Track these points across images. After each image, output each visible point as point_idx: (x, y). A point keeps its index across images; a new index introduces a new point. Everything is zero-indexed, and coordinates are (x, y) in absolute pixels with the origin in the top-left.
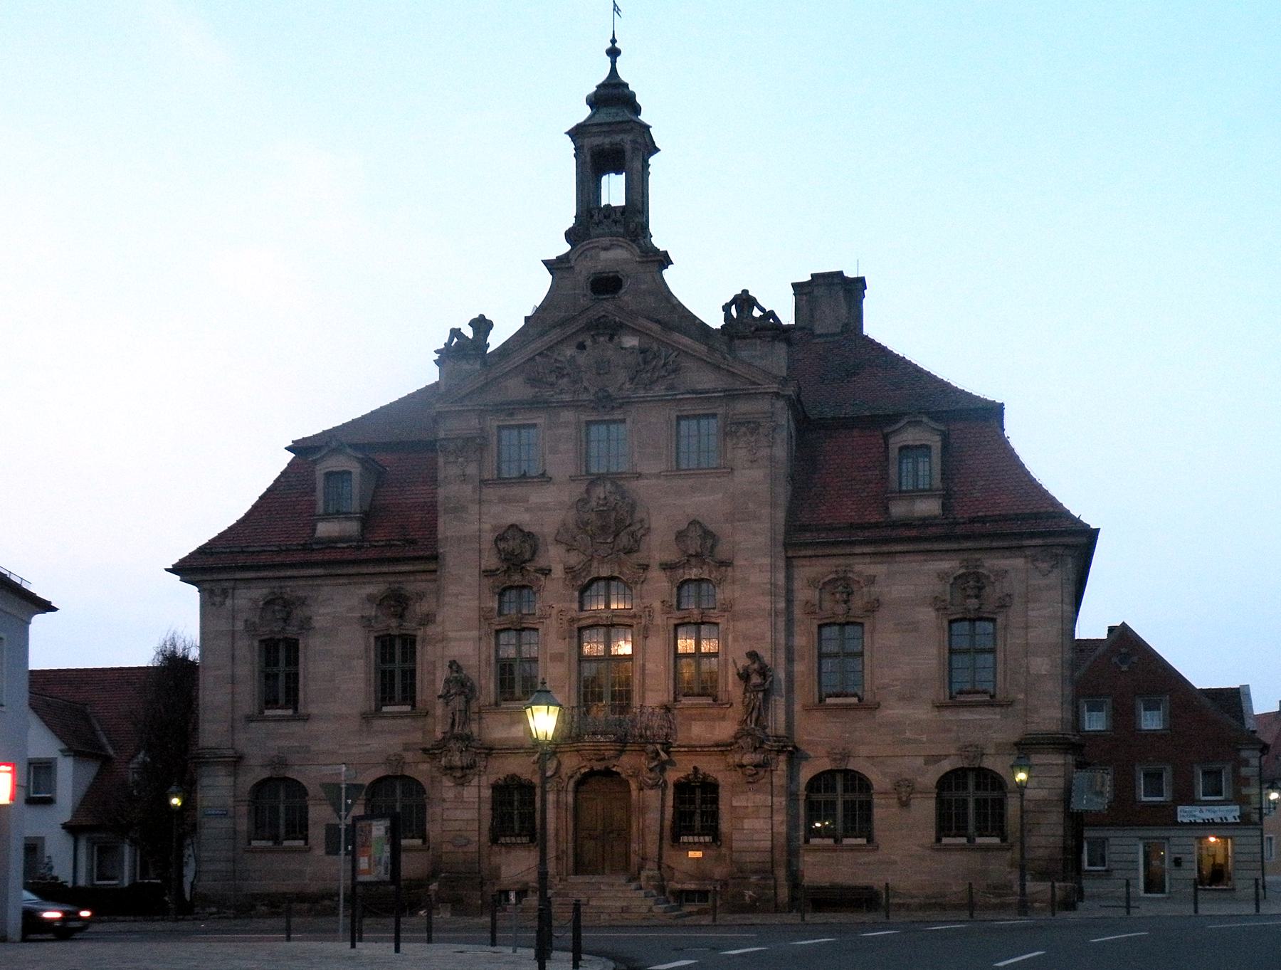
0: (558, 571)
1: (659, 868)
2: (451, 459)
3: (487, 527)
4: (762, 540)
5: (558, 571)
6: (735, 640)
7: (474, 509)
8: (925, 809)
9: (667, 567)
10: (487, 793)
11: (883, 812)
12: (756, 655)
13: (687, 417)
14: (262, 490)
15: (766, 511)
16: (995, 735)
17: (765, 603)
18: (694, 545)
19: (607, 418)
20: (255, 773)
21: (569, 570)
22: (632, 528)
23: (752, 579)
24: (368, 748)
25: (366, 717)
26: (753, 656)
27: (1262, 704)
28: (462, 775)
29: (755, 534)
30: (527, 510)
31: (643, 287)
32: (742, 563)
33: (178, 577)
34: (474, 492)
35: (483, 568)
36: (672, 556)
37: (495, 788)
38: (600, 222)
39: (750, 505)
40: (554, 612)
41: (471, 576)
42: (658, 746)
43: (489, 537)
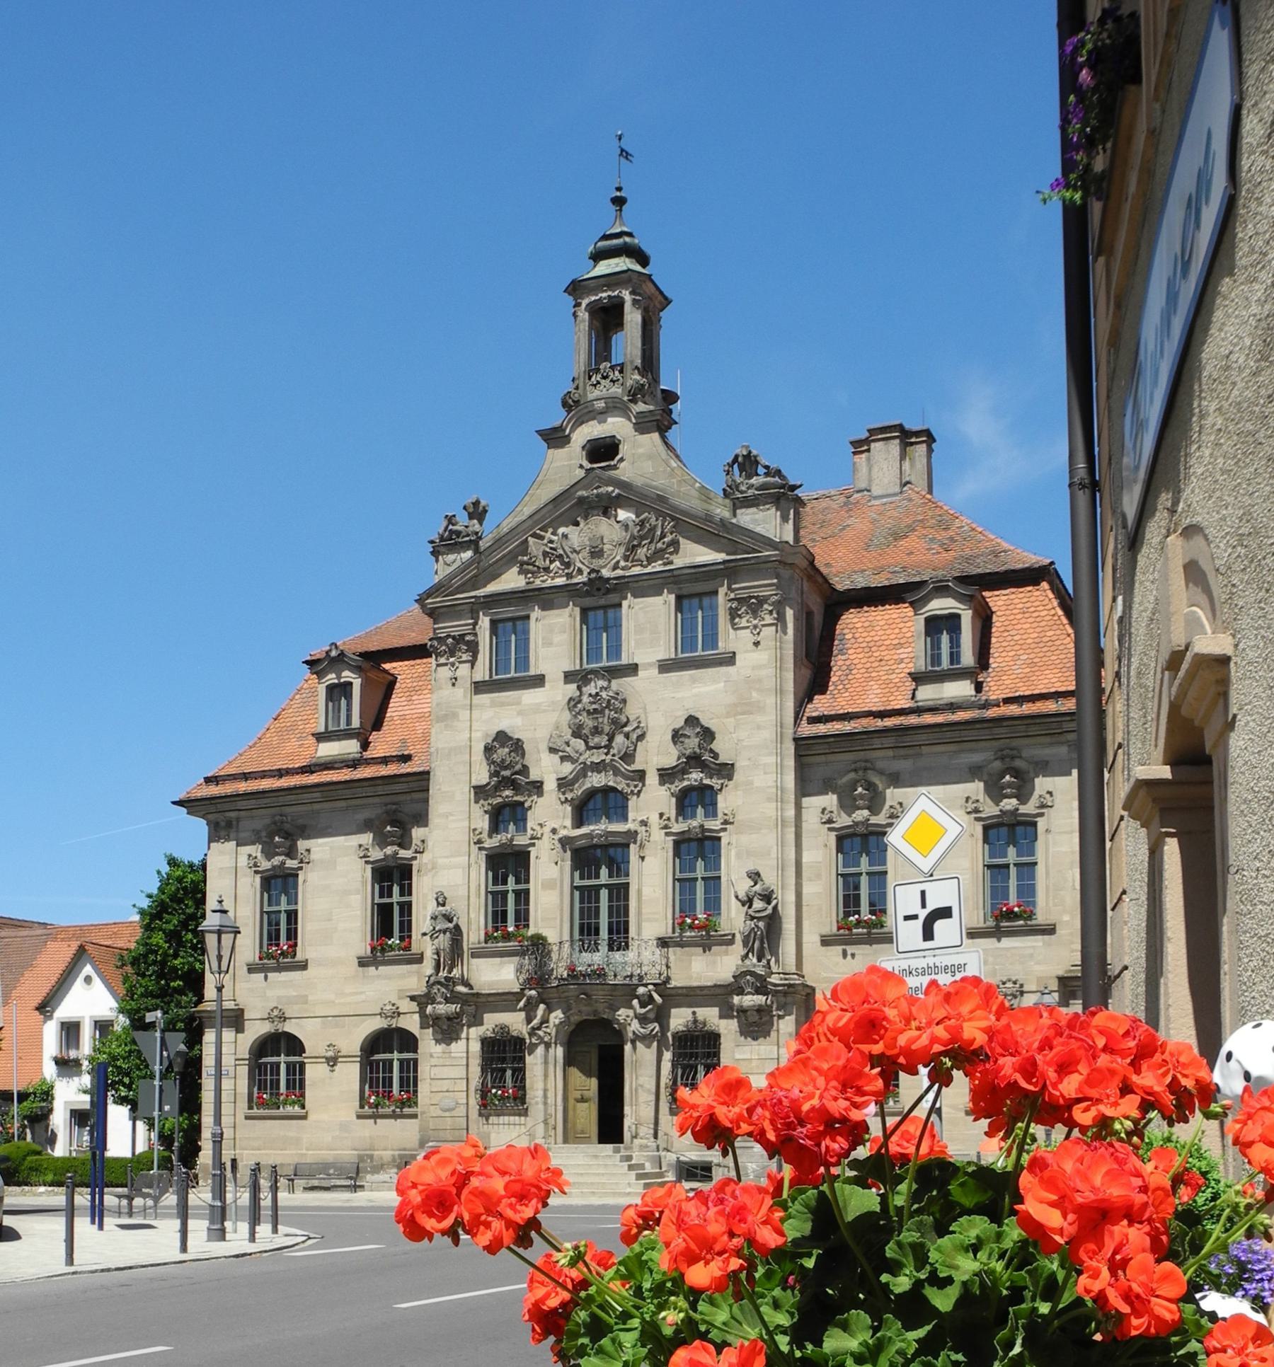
0: (550, 785)
1: (656, 1136)
2: (442, 660)
3: (477, 735)
4: (768, 734)
5: (550, 785)
6: (738, 856)
7: (464, 714)
8: (350, 1073)
9: (666, 775)
10: (476, 1047)
11: (314, 1073)
12: (758, 874)
13: (691, 596)
14: (1187, 985)
15: (771, 700)
16: (1037, 968)
17: (770, 809)
18: (692, 744)
19: (602, 602)
20: (256, 1030)
21: (563, 784)
22: (626, 729)
23: (757, 783)
24: (363, 997)
25: (363, 963)
26: (755, 876)
27: (1106, 5)
28: (447, 1030)
29: (759, 727)
30: (520, 713)
31: (641, 451)
32: (746, 763)
33: (185, 810)
34: (465, 697)
35: (474, 783)
36: (670, 758)
37: (485, 1041)
38: (598, 383)
39: (754, 694)
40: (547, 830)
41: (463, 793)
42: (651, 987)
43: (479, 748)
